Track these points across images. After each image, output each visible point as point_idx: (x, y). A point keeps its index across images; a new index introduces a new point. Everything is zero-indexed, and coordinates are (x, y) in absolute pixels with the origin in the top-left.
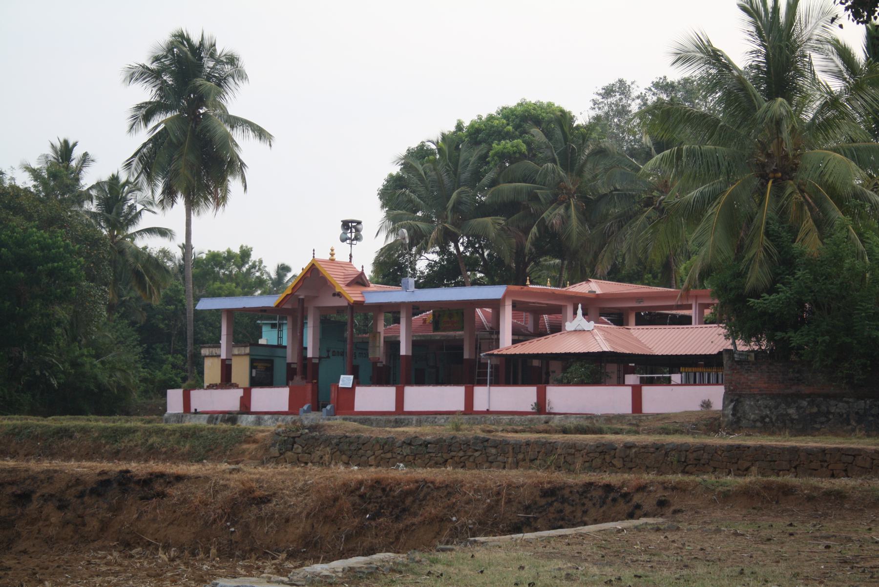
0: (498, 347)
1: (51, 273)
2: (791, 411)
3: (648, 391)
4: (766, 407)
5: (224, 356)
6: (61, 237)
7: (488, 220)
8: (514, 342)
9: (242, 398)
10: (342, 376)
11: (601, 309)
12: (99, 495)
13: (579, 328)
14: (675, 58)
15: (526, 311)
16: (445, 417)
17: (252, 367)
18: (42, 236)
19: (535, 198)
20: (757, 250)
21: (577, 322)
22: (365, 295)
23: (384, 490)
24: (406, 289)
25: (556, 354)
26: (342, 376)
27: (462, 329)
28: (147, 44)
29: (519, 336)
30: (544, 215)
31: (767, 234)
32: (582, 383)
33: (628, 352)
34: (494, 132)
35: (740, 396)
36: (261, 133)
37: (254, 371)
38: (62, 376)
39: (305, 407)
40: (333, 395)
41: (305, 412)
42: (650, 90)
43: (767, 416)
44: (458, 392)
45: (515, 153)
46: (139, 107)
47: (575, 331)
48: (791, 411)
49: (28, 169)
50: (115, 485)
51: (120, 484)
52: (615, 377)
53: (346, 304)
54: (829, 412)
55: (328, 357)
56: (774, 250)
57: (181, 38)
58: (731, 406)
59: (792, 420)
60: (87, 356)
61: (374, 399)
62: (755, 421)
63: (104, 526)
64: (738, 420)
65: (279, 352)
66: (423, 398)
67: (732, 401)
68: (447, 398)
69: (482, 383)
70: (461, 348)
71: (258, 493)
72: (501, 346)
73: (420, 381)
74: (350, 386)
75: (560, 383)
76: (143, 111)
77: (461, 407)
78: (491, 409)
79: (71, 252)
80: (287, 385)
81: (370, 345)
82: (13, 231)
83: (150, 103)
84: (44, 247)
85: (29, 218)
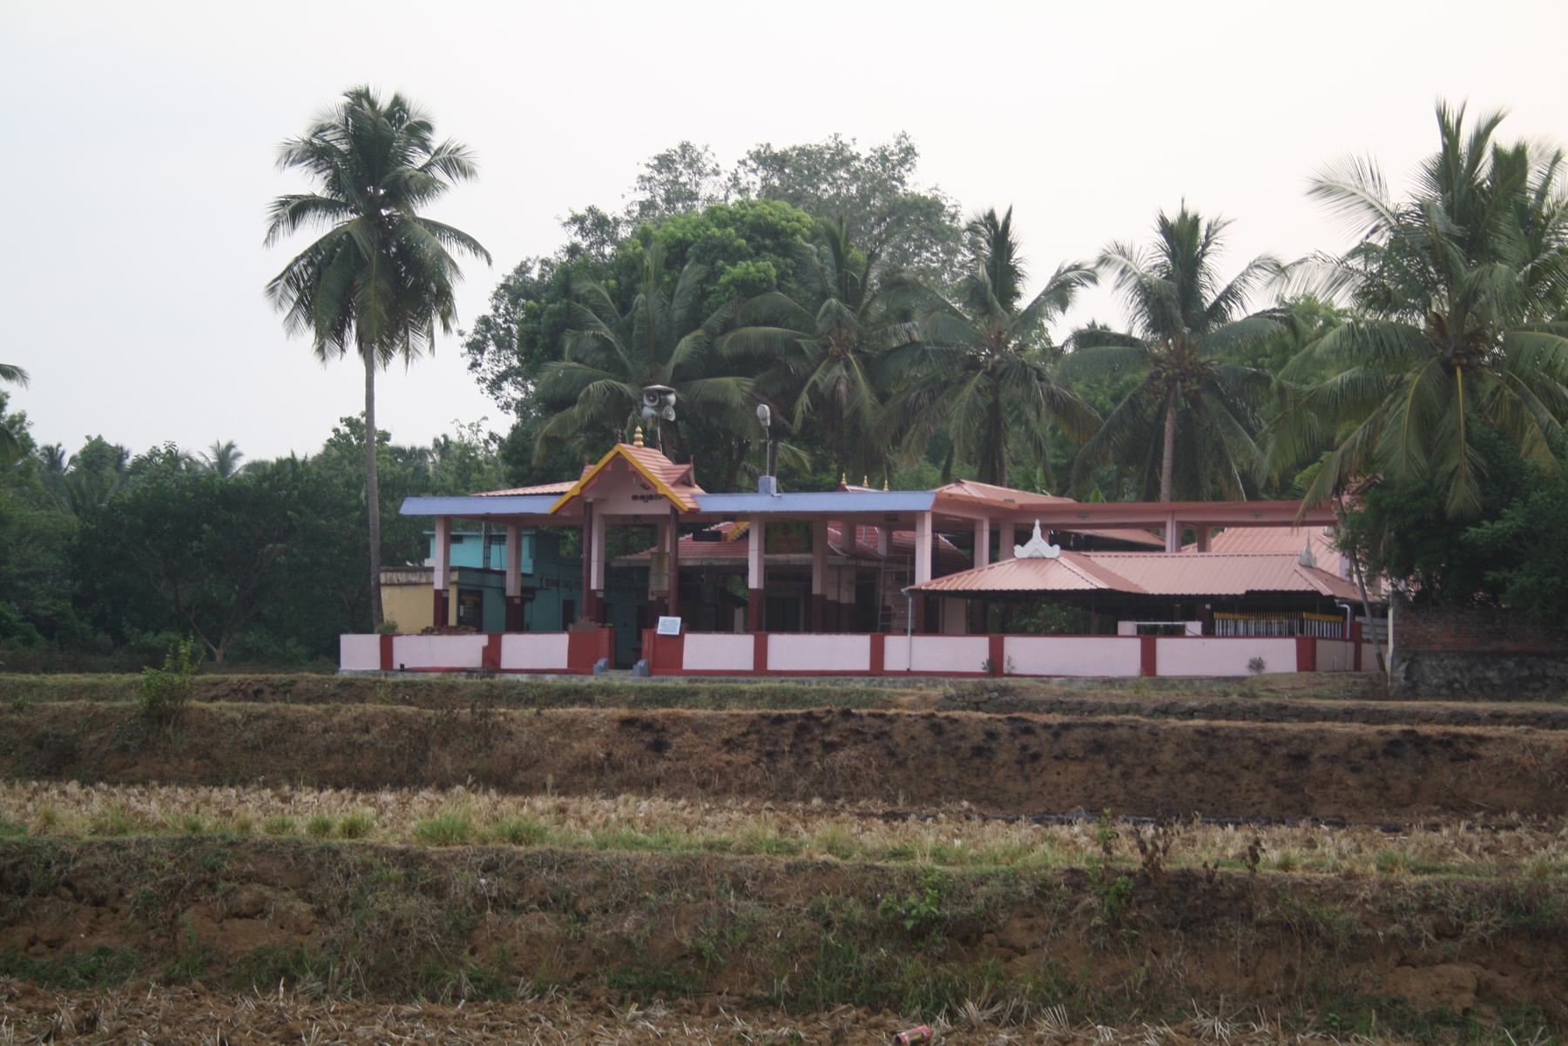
2: (1490, 674)
3: (1164, 645)
4: (1454, 668)
5: (439, 585)
7: (729, 380)
8: (935, 575)
9: (485, 650)
10: (662, 619)
13: (1036, 554)
14: (1311, 187)
16: (832, 679)
19: (797, 351)
20: (1460, 458)
24: (767, 492)
25: (1016, 592)
26: (662, 619)
27: (809, 549)
28: (319, 102)
30: (814, 377)
31: (1469, 439)
32: (1060, 633)
34: (715, 246)
35: (1416, 653)
36: (475, 246)
40: (647, 645)
41: (602, 669)
42: (743, 163)
43: (1456, 680)
45: (761, 281)
46: (283, 204)
47: (1030, 558)
48: (1490, 674)
53: (667, 511)
54: (1545, 676)
56: (1482, 461)
57: (361, 97)
58: (1403, 667)
59: (1492, 686)
61: (716, 652)
62: (1438, 687)
63: (1416, 789)
64: (1415, 686)
65: (493, 580)
66: (797, 651)
67: (1404, 660)
68: (844, 652)
70: (809, 579)
75: (1022, 631)
77: (865, 665)
78: (914, 669)
80: (564, 629)
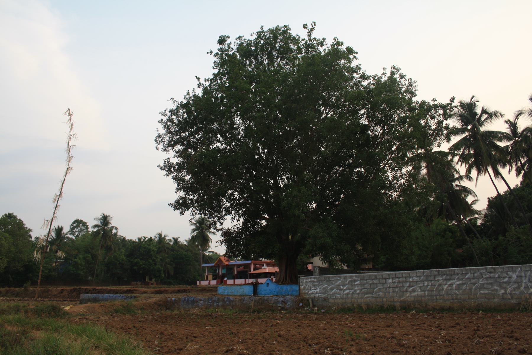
21: (265, 267)
29: (255, 269)
44: (244, 280)
85: (184, 250)
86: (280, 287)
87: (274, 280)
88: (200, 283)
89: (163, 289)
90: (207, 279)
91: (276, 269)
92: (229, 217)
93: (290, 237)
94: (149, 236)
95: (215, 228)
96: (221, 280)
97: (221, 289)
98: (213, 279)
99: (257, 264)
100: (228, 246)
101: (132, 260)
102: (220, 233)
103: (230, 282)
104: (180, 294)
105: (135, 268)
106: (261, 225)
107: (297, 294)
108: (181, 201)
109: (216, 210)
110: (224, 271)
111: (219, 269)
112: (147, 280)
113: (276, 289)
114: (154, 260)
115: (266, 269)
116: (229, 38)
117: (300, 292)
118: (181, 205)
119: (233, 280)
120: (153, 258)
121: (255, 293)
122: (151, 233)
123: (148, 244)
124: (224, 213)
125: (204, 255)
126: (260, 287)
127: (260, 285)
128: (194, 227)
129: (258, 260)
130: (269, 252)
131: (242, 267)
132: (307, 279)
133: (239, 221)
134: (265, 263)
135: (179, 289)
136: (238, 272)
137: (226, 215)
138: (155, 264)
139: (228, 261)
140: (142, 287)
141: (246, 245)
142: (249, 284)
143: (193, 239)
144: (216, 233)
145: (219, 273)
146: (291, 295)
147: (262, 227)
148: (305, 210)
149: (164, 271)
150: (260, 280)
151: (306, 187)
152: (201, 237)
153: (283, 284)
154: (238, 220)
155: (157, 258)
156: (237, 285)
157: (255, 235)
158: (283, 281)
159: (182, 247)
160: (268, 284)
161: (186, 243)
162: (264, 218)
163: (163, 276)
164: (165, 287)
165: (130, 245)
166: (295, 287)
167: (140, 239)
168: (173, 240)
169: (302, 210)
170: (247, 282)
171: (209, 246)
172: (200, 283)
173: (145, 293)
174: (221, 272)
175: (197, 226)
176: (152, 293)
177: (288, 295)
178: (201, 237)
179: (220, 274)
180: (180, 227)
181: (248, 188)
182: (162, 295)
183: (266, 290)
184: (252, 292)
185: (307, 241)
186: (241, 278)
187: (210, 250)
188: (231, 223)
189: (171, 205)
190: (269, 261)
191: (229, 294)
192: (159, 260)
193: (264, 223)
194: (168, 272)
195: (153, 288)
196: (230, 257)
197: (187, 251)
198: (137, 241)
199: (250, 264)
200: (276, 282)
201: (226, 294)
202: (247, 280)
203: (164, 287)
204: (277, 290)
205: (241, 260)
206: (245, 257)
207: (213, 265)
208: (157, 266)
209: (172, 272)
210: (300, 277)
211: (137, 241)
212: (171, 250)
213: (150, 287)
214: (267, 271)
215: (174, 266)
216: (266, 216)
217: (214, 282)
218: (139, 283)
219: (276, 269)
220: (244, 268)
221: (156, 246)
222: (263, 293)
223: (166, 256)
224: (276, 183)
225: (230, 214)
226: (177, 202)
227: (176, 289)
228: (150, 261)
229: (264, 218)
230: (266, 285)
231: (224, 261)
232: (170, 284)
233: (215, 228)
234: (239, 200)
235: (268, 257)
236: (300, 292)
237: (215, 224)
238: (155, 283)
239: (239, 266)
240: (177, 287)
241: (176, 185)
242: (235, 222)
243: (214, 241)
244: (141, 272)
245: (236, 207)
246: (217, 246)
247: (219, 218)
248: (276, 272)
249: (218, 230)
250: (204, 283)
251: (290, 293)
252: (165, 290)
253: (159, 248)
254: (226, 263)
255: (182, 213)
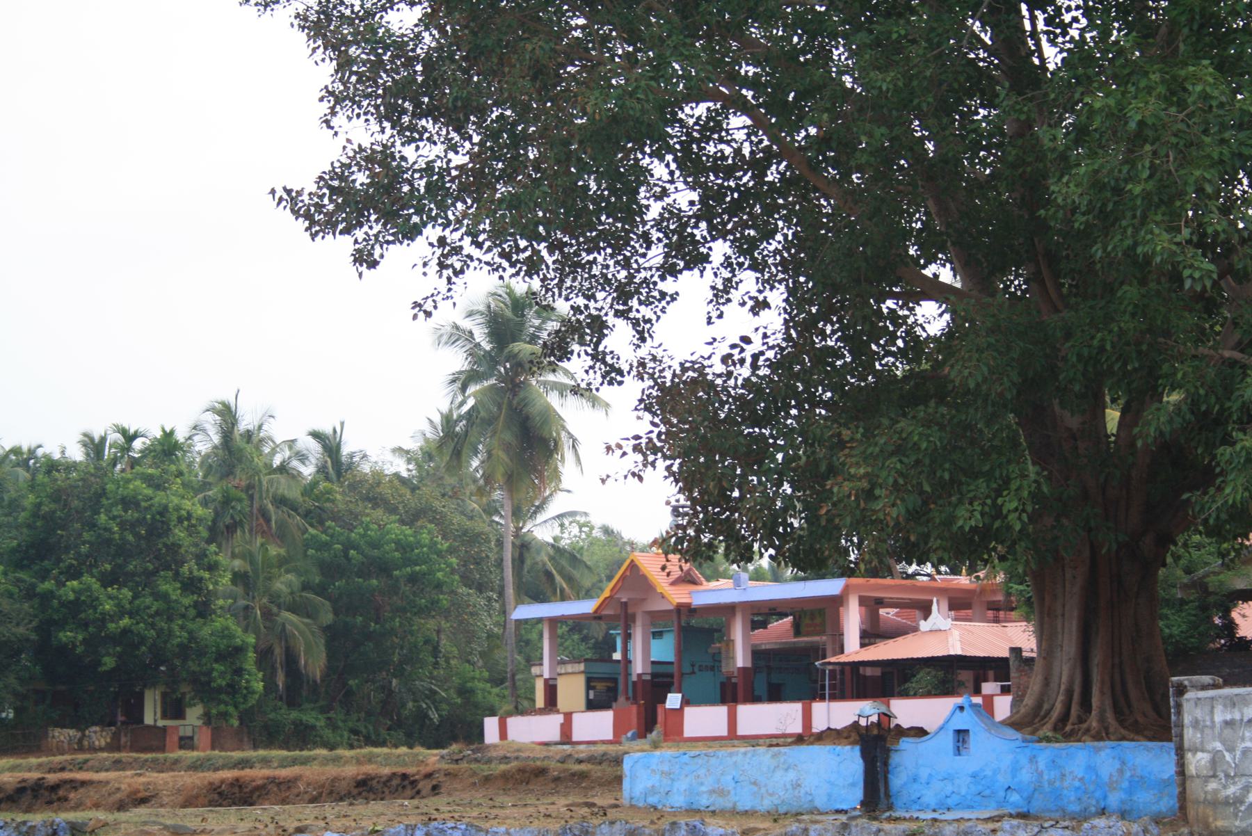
0: (842, 652)
1: (413, 579)
5: (546, 676)
6: (427, 533)
9: (562, 725)
11: (989, 603)
12: (14, 801)
13: (935, 628)
15: (913, 607)
17: (589, 687)
18: (402, 532)
21: (939, 618)
22: (694, 595)
23: (240, 787)
29: (869, 636)
32: (928, 694)
33: (982, 655)
37: (592, 693)
38: (444, 706)
39: (629, 734)
44: (795, 709)
49: (399, 451)
50: (29, 792)
51: (33, 790)
52: (971, 685)
53: (671, 607)
55: (693, 673)
60: (479, 680)
69: (822, 698)
71: (140, 795)
72: (846, 651)
73: (754, 699)
74: (678, 706)
76: (458, 384)
79: (439, 554)
81: (723, 656)
82: (367, 529)
83: (460, 373)
84: (401, 546)
85: (393, 510)
86: (1046, 753)
87: (1003, 706)
88: (503, 734)
89: (258, 774)
90: (551, 703)
91: (1017, 636)
92: (692, 287)
93: (1113, 416)
94: (149, 426)
95: (598, 357)
96: (643, 705)
97: (648, 773)
98: (592, 706)
99: (880, 602)
100: (686, 480)
101: (48, 585)
102: (633, 388)
103: (704, 720)
104: (376, 806)
105: (66, 636)
106: (910, 332)
107: (1168, 803)
108: (361, 178)
109: (603, 235)
110: (664, 650)
111: (627, 637)
112: (151, 715)
113: (1015, 770)
114: (191, 585)
115: (944, 635)
116: (293, 441)
117: (1183, 796)
118: (362, 204)
119: (721, 711)
120: (189, 568)
121: (876, 793)
122: (164, 401)
123: (149, 480)
124: (656, 255)
125: (524, 547)
126: (906, 757)
127: (906, 744)
128: (457, 360)
129: (890, 573)
130: (968, 517)
131: (781, 627)
132: (1232, 703)
133: (765, 305)
134: (941, 591)
135: (370, 769)
136: (757, 654)
137: (669, 270)
138: (203, 611)
139: (687, 580)
140: (118, 765)
141: (812, 477)
142: (830, 736)
143: (452, 441)
144: (606, 392)
145: (627, 662)
146: (1123, 815)
147: (915, 346)
148: (1216, 223)
149: (264, 656)
150: (907, 711)
151: (1223, 67)
152: (509, 432)
153: (1068, 737)
154: (760, 306)
155: (212, 567)
156: (753, 740)
157: (867, 405)
158: (1064, 718)
159: (374, 491)
160: (961, 734)
161: (401, 467)
162: (935, 290)
163: (259, 686)
164: (269, 763)
165: (32, 486)
166: (1151, 759)
167: (94, 446)
168: (314, 447)
169: (1199, 226)
170: (819, 725)
171: (556, 476)
172: (503, 734)
173: (143, 801)
174: (644, 652)
175: (474, 352)
176: (189, 802)
177: (1102, 812)
178: (509, 432)
179: (638, 667)
180: (357, 361)
181: (820, 87)
182: (257, 811)
183: (948, 778)
184: (858, 794)
185: (1228, 441)
186: (775, 695)
187: (558, 504)
188: (718, 320)
189: (291, 198)
190: (963, 581)
191: (704, 801)
192: (226, 579)
193: (931, 318)
194: (291, 660)
195: (195, 767)
196: (698, 554)
197: (412, 518)
198: (77, 454)
199: (837, 602)
200: (1014, 723)
201: (678, 800)
202: (819, 708)
203: (266, 762)
204: (1026, 776)
205: (776, 578)
206: (808, 557)
207: (586, 607)
208: (219, 623)
209: (314, 662)
210: (1181, 690)
211: (77, 454)
212: (307, 515)
213: (174, 765)
214: (956, 649)
215: (328, 617)
216: (946, 275)
217: (596, 726)
218: (98, 736)
219: (1017, 636)
220: (797, 629)
221: (205, 486)
222: (930, 797)
223: (274, 551)
224: (1013, 45)
225: (698, 260)
226: (336, 182)
227: (350, 771)
228: (169, 587)
229: (935, 290)
230: (948, 740)
231: (661, 582)
232: (302, 737)
233: (598, 357)
234: (758, 167)
235: (965, 550)
236: (1183, 796)
237: (599, 326)
238: (204, 737)
239: (761, 614)
240: (351, 762)
241: (324, 72)
242: (737, 321)
243: (591, 448)
244: (109, 662)
245: (734, 208)
246: (612, 487)
247: (624, 293)
248: (1016, 651)
249: (613, 374)
250: (532, 731)
251: (1114, 800)
252: (272, 780)
253: (227, 501)
254: (679, 596)
255: (365, 259)
